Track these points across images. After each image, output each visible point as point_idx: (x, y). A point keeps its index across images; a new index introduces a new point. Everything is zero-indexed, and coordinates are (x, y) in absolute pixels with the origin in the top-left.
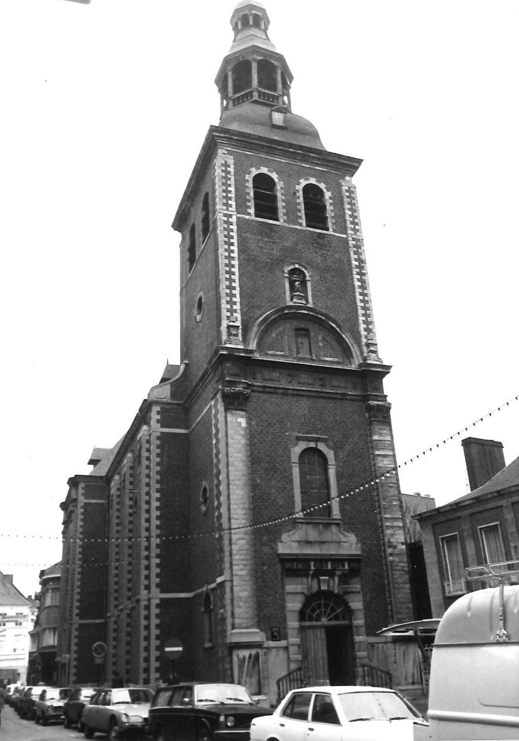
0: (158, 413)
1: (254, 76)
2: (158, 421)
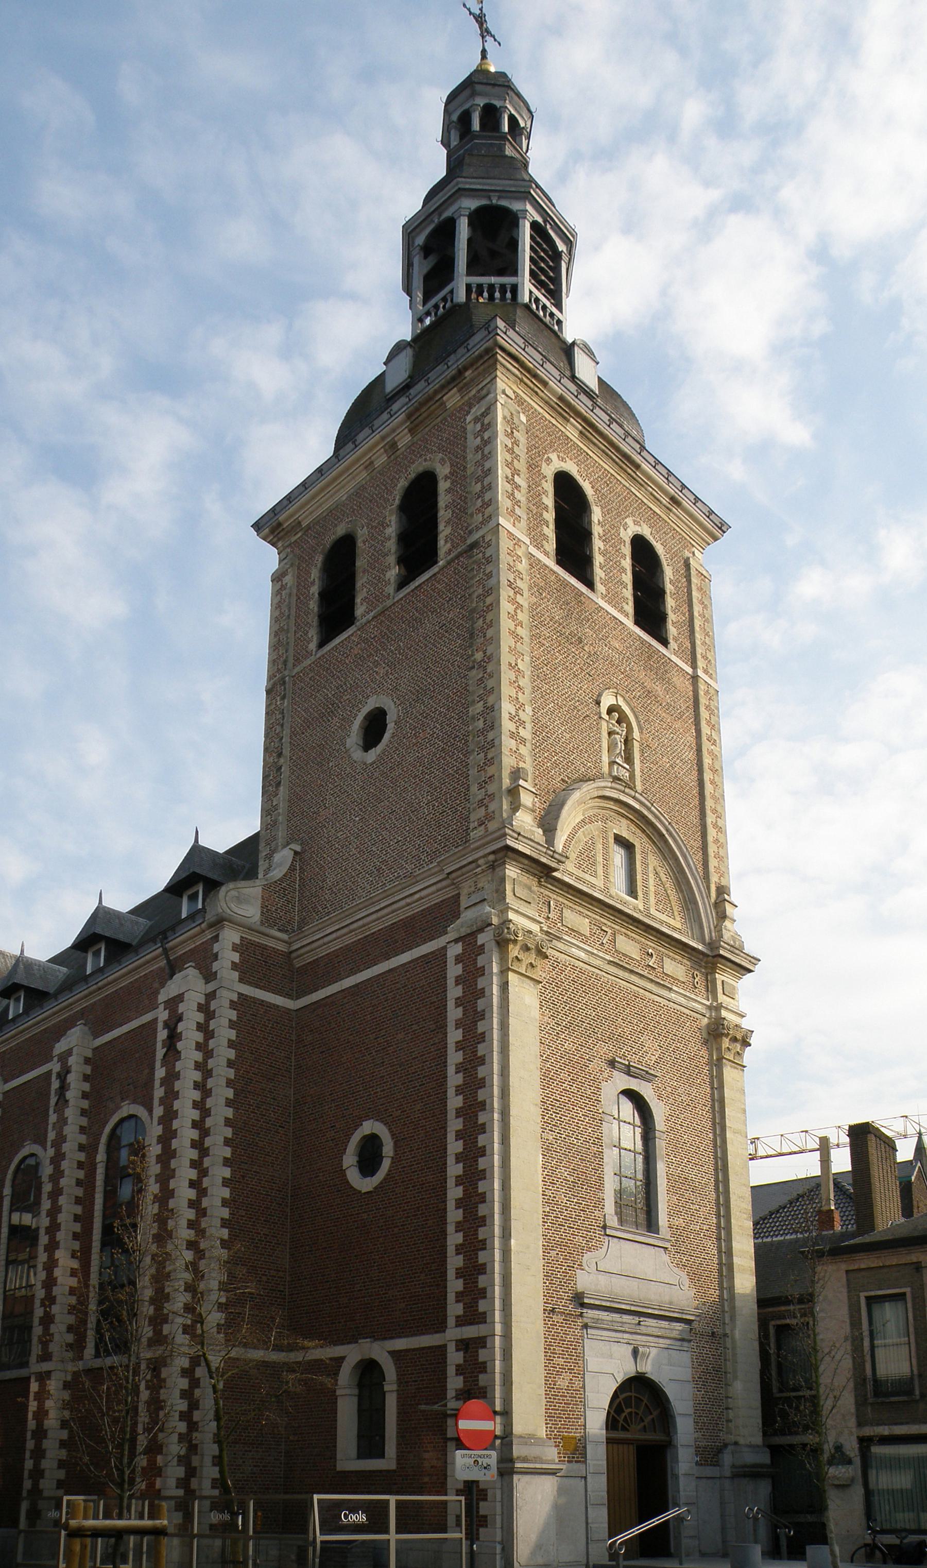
0: (235, 948)
1: (483, 121)
2: (235, 967)
